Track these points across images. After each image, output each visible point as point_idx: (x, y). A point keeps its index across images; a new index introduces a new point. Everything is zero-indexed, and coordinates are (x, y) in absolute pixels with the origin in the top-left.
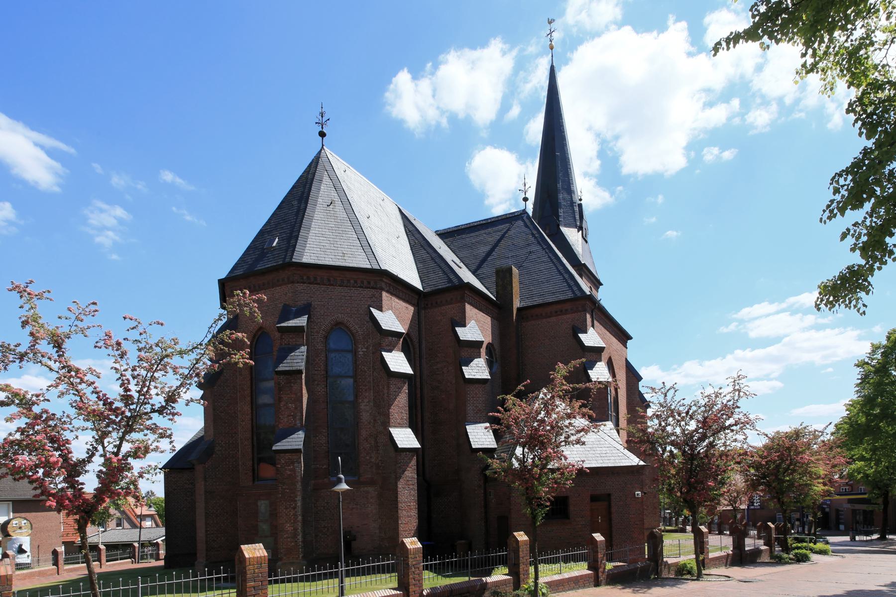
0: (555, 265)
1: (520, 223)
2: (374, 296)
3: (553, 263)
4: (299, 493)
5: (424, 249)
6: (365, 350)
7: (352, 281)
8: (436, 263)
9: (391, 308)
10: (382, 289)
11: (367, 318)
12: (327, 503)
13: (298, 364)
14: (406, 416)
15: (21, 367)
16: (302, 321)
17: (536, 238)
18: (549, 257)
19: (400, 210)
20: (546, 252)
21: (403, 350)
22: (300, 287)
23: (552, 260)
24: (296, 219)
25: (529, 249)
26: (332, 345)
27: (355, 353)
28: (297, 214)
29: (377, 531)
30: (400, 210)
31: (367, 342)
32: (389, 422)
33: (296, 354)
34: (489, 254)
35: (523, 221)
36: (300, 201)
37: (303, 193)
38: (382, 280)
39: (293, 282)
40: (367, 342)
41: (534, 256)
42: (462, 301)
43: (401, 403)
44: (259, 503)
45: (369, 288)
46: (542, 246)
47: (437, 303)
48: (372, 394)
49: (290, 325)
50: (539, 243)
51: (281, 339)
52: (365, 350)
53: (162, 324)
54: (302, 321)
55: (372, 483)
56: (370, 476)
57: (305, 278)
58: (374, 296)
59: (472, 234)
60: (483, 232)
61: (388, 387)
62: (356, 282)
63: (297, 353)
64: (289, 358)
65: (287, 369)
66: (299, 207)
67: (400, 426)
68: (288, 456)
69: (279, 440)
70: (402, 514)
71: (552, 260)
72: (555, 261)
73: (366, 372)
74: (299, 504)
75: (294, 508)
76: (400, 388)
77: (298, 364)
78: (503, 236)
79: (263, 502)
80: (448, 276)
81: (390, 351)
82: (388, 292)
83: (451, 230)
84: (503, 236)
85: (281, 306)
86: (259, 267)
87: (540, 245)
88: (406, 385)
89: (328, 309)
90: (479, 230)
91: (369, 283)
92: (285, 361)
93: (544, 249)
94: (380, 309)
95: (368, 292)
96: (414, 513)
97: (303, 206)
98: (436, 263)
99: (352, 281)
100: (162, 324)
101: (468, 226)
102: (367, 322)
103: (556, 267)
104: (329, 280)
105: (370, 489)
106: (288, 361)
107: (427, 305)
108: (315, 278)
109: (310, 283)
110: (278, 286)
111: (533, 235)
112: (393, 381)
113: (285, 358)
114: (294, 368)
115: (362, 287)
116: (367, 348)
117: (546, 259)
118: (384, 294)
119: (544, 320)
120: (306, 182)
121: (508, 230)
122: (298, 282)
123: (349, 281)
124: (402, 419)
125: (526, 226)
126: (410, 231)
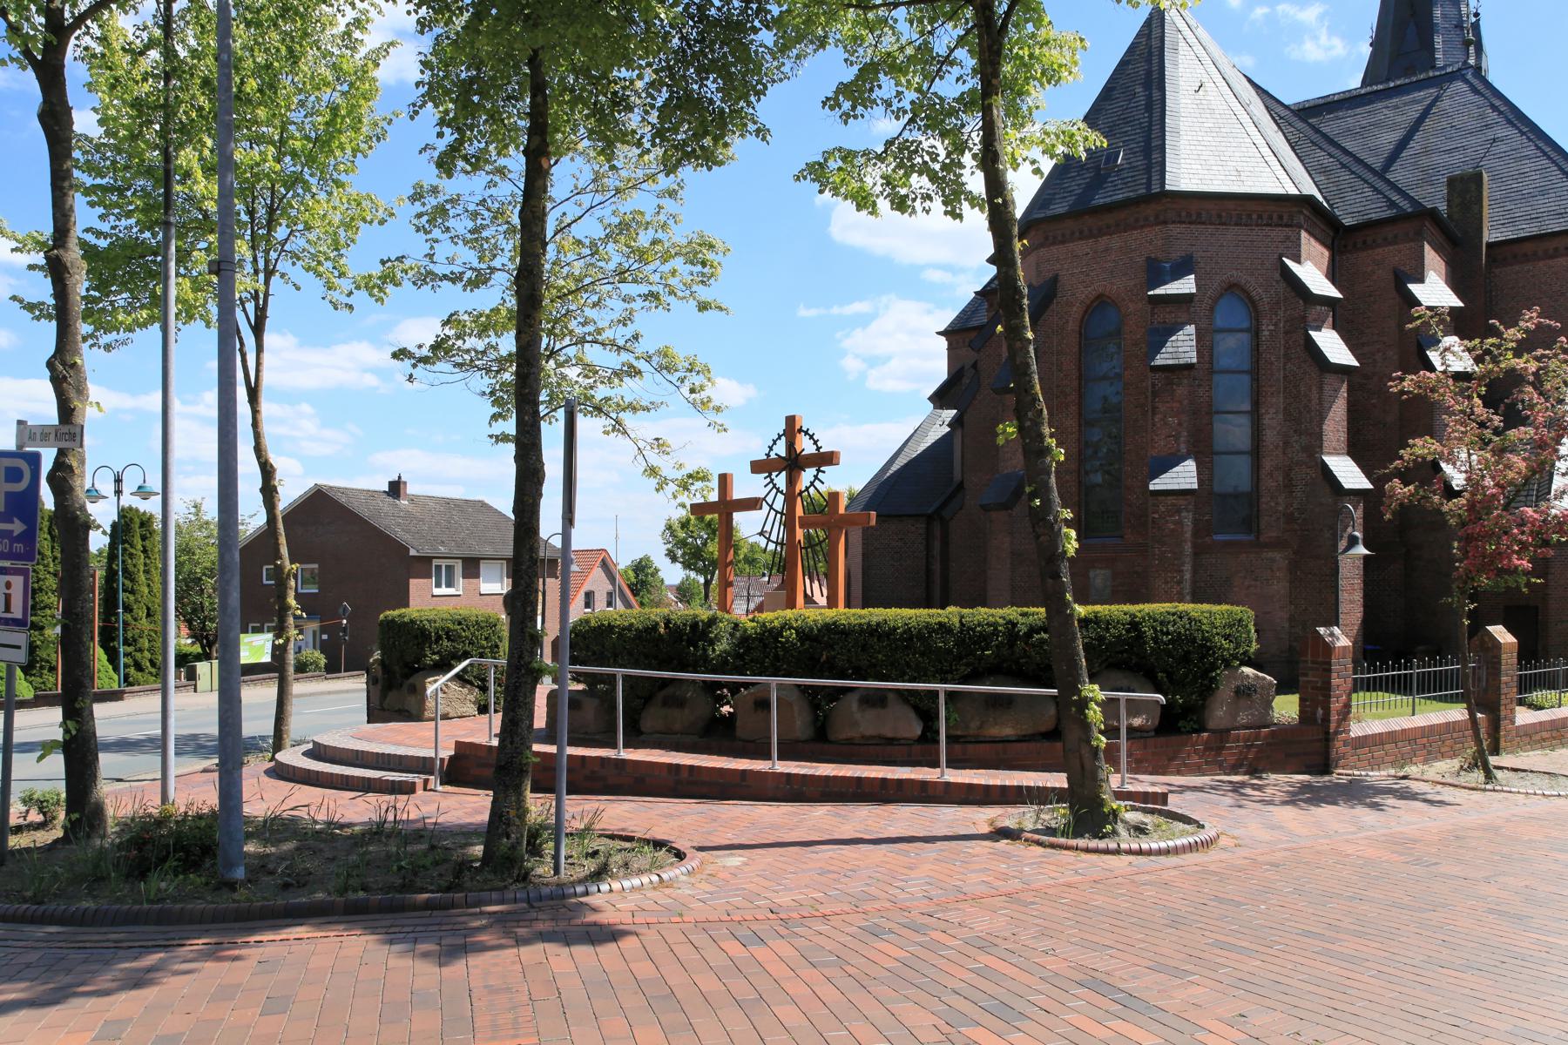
0: (1554, 162)
1: (1459, 86)
2: (1288, 238)
3: (1549, 158)
4: (1188, 560)
5: (1320, 148)
6: (1272, 328)
7: (1254, 216)
8: (1353, 173)
9: (1309, 258)
10: (1300, 227)
11: (1277, 276)
12: (1211, 576)
13: (1187, 355)
14: (1343, 436)
15: (411, 378)
16: (1186, 285)
17: (1501, 113)
18: (1538, 148)
19: (1250, 81)
20: (1528, 138)
21: (1334, 328)
22: (1176, 230)
23: (1545, 154)
24: (1150, 117)
25: (1490, 134)
26: (1219, 322)
27: (1256, 333)
28: (1149, 107)
29: (1287, 625)
30: (1250, 81)
31: (1276, 315)
32: (1321, 447)
33: (1180, 338)
34: (1402, 145)
35: (1467, 81)
36: (1147, 85)
37: (1149, 73)
38: (1301, 212)
39: (1165, 223)
40: (1276, 315)
41: (1504, 148)
42: (1418, 238)
43: (1337, 414)
44: (1091, 574)
45: (1281, 225)
46: (1517, 128)
47: (1364, 242)
48: (1282, 400)
49: (1169, 292)
50: (1510, 122)
51: (1153, 314)
52: (1272, 328)
53: (298, 289)
54: (1186, 285)
55: (1277, 544)
56: (1274, 534)
57: (1184, 214)
58: (1288, 238)
59: (1358, 110)
60: (1380, 105)
61: (1321, 389)
62: (1260, 217)
63: (1180, 336)
64: (1168, 344)
65: (1170, 362)
66: (1149, 97)
67: (1336, 452)
68: (1170, 500)
69: (1156, 474)
70: (1343, 596)
71: (1545, 154)
72: (1552, 154)
73: (1272, 363)
74: (1188, 576)
75: (1179, 583)
76: (1337, 391)
77: (1187, 355)
78: (1425, 114)
79: (1098, 571)
80: (1385, 197)
81: (1318, 329)
82: (1306, 230)
83: (1312, 104)
84: (1425, 114)
85: (1141, 260)
86: (1100, 199)
87: (1514, 125)
88: (1345, 385)
89: (1217, 263)
90: (1371, 102)
91: (1281, 217)
92: (1164, 350)
93: (1523, 134)
94: (1298, 260)
95: (1278, 233)
96: (1358, 596)
97: (1156, 94)
98: (1353, 173)
99: (1254, 216)
100: (298, 289)
101: (1347, 95)
102: (1277, 282)
103: (1557, 165)
104: (1219, 216)
105: (1277, 555)
106: (1170, 350)
107: (1345, 246)
108: (1199, 215)
109: (1190, 223)
110: (1135, 228)
111: (1494, 108)
112: (1329, 379)
113: (1163, 345)
114: (1182, 361)
115: (1270, 225)
116: (1276, 325)
117: (1530, 150)
118: (1304, 234)
119: (1541, 264)
120: (1150, 54)
121: (1437, 99)
122: (1173, 222)
123: (1249, 216)
124: (1338, 441)
125: (1475, 91)
126: (1281, 118)
